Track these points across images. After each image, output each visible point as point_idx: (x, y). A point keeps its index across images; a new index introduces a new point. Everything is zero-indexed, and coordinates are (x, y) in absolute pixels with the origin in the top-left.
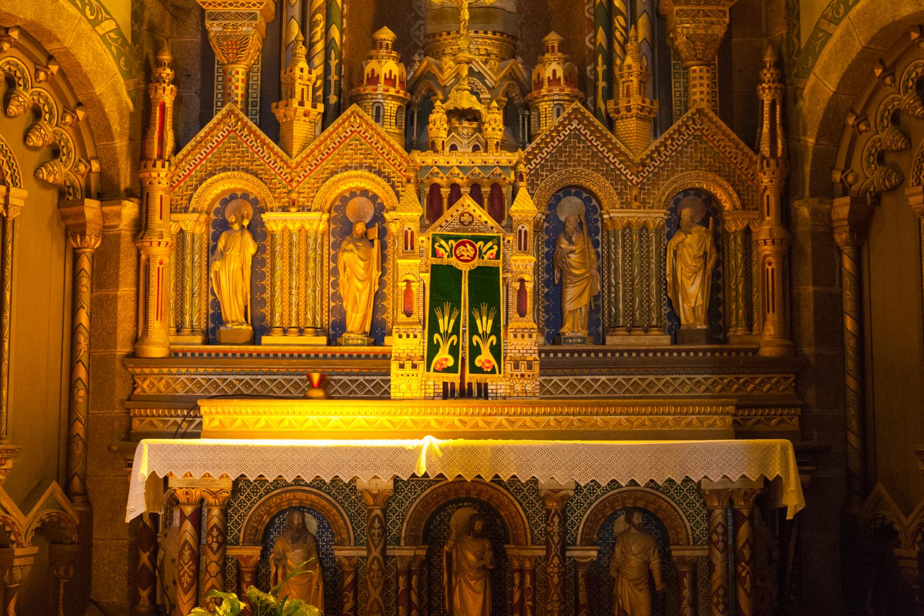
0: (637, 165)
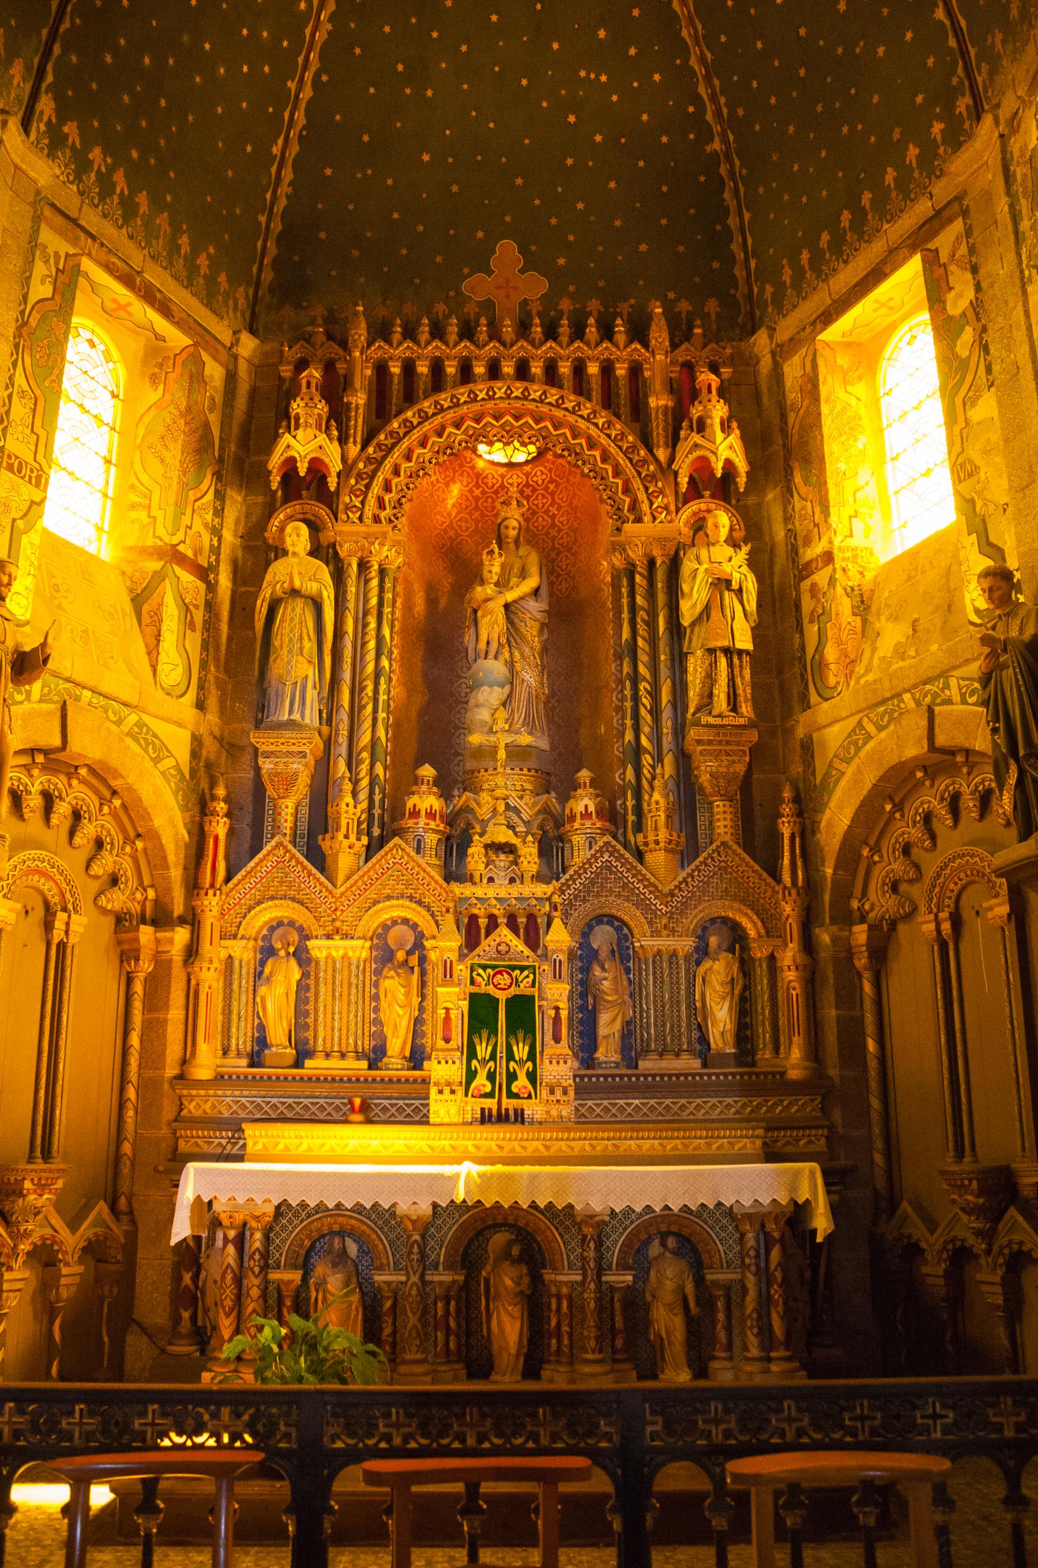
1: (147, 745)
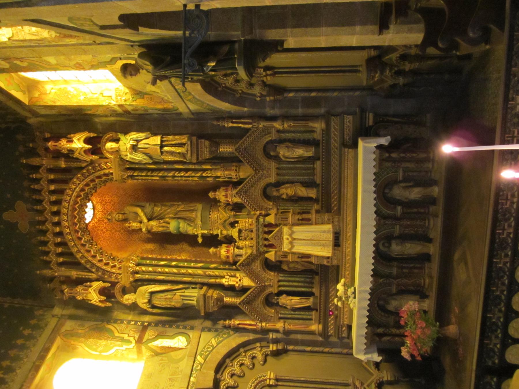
0: (256, 172)
1: (208, 351)
